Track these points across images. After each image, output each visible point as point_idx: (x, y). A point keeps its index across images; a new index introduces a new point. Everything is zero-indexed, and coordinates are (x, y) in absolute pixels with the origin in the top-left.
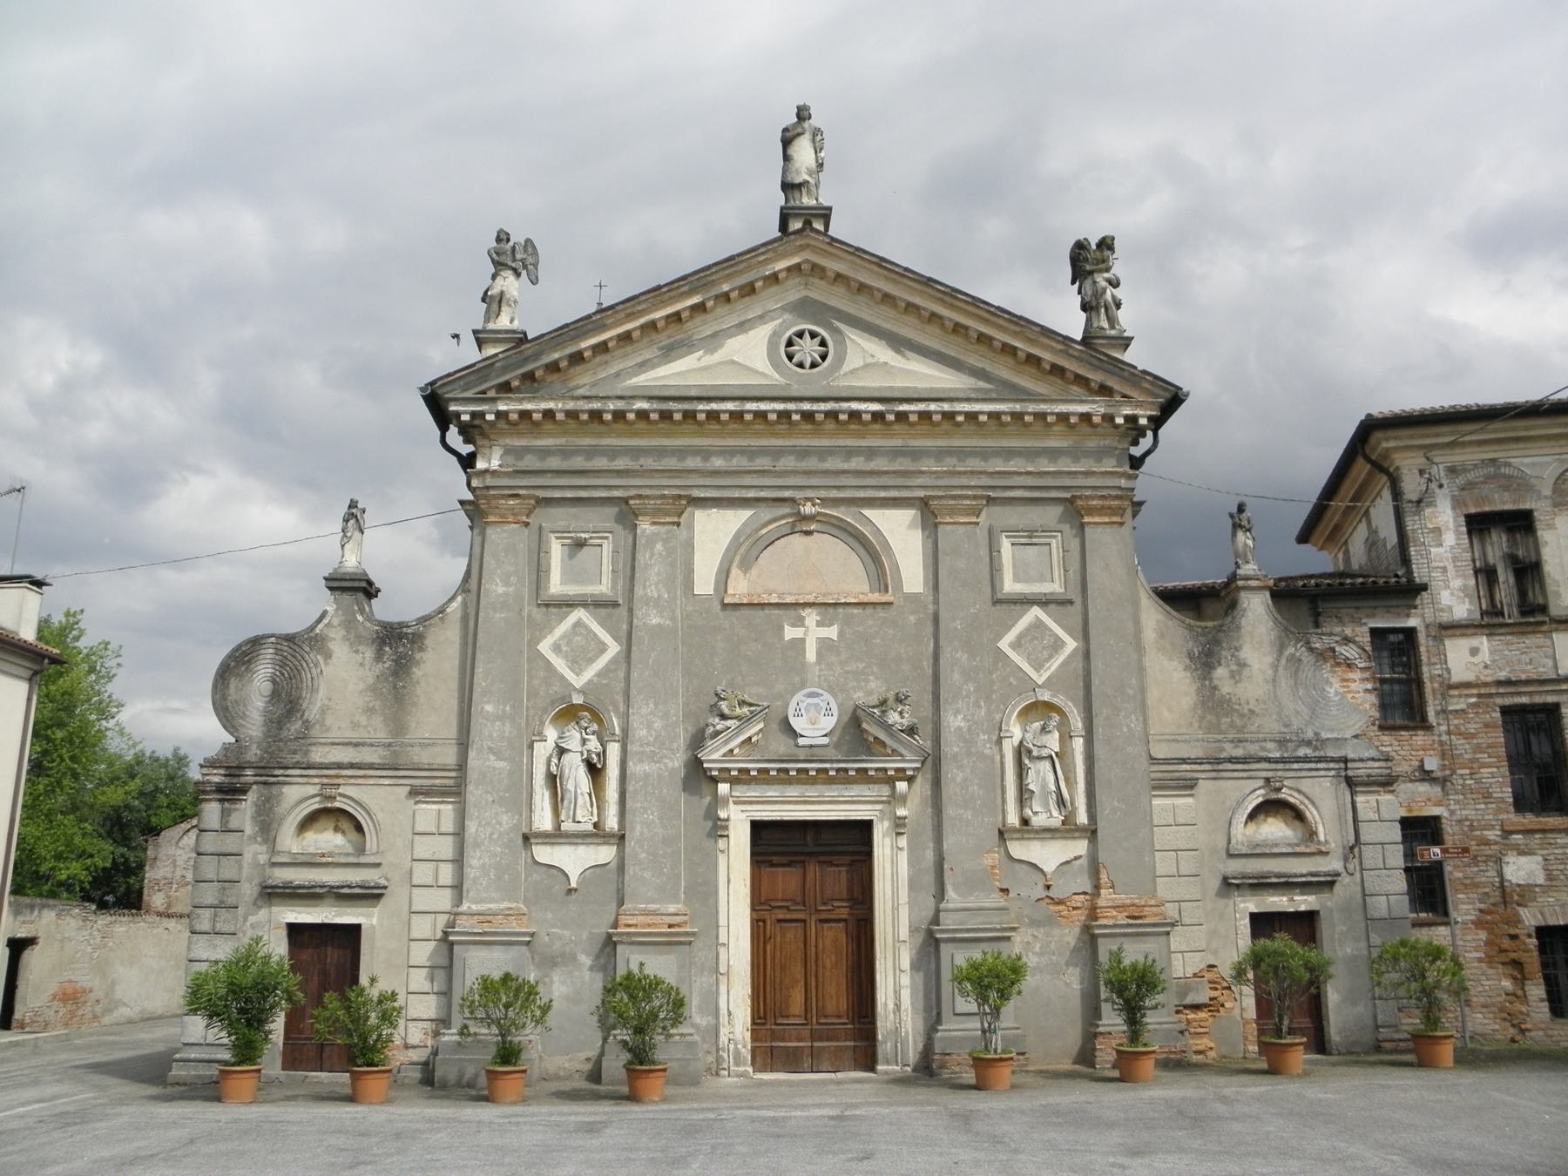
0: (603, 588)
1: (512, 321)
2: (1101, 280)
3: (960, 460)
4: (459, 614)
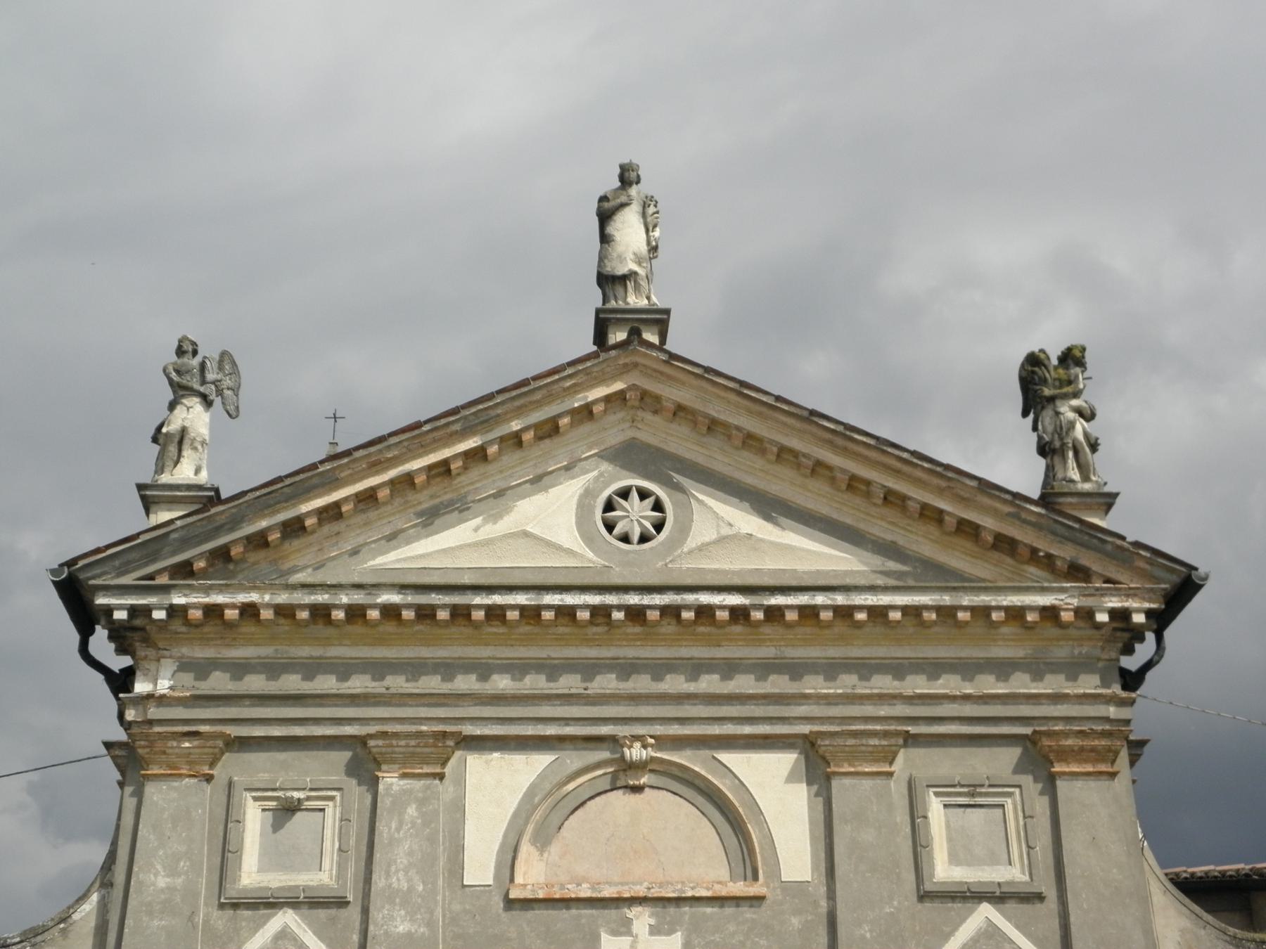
0: (323, 877)
1: (197, 471)
2: (1066, 410)
3: (862, 678)
4: (92, 923)
